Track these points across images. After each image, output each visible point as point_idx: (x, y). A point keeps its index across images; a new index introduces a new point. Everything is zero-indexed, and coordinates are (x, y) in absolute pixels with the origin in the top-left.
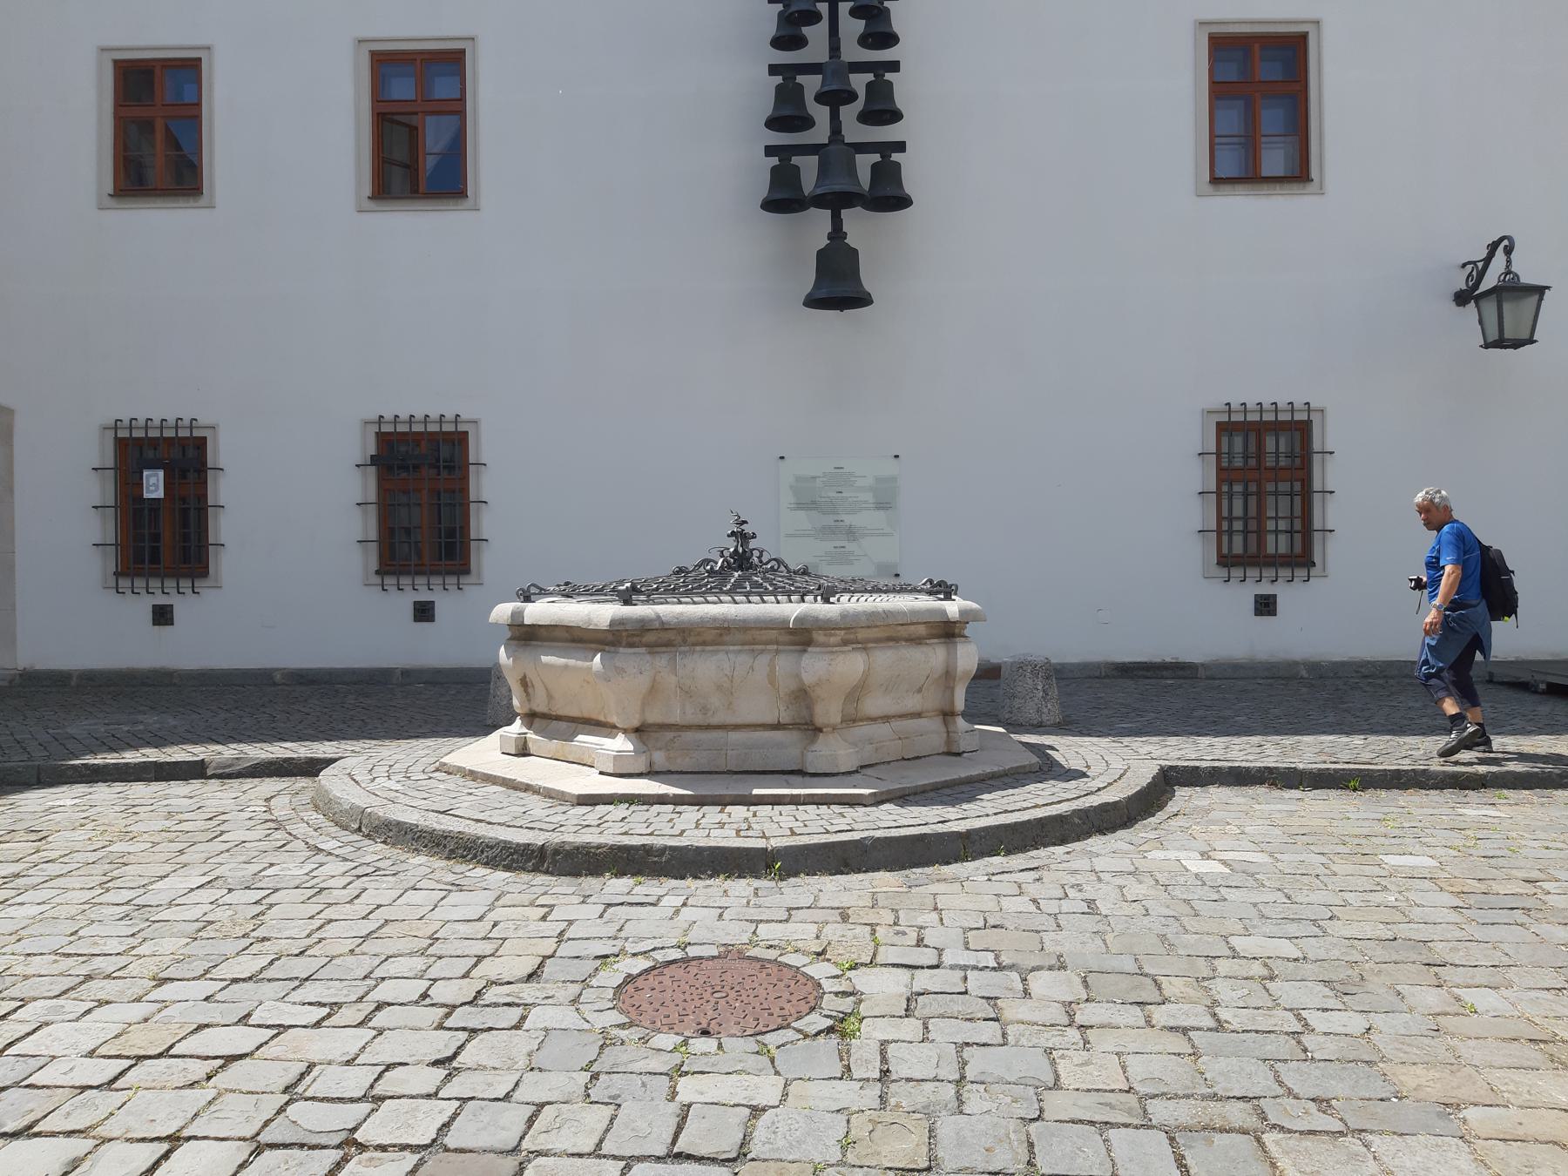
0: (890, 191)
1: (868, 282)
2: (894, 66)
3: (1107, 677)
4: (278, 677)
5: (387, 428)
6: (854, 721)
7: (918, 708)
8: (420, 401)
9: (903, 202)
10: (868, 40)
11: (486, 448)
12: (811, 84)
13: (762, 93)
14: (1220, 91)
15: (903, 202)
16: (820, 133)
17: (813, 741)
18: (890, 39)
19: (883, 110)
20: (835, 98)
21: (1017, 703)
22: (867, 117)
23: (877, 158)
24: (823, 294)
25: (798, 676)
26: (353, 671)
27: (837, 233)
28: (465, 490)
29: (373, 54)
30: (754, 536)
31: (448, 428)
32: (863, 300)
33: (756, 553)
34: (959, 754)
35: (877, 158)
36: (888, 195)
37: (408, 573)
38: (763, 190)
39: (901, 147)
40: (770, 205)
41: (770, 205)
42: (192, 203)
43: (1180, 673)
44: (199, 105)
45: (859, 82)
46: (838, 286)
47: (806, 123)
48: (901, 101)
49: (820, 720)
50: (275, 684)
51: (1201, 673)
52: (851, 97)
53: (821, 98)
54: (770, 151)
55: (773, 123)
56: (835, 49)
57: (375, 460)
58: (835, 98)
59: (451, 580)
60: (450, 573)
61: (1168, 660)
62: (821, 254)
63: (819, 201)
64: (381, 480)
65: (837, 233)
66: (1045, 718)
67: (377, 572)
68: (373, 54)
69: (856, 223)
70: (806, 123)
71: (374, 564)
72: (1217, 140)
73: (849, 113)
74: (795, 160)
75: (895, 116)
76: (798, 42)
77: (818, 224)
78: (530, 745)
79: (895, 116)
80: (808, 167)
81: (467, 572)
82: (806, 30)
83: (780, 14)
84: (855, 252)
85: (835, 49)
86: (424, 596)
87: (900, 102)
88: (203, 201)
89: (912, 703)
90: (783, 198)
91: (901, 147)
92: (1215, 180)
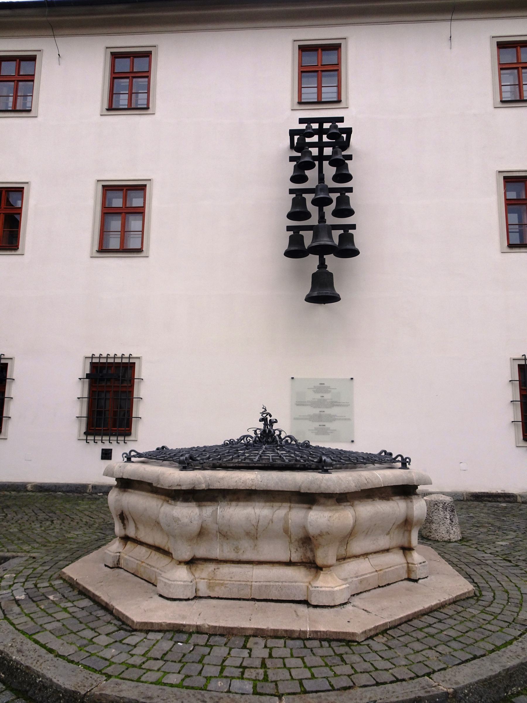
0: (349, 247)
1: (338, 289)
2: (350, 190)
3: (468, 500)
4: (29, 487)
5: (95, 361)
6: (344, 559)
7: (387, 547)
8: (112, 348)
9: (355, 253)
10: (337, 178)
11: (143, 371)
12: (309, 197)
13: (286, 203)
14: (510, 204)
15: (355, 253)
16: (314, 220)
17: (316, 576)
18: (348, 178)
19: (344, 210)
20: (321, 203)
21: (434, 526)
22: (337, 213)
23: (342, 232)
24: (315, 294)
25: (313, 579)
26: (68, 485)
27: (322, 265)
28: (131, 392)
29: (104, 186)
30: (276, 421)
31: (125, 361)
32: (335, 298)
33: (277, 433)
34: (416, 581)
35: (342, 232)
36: (347, 250)
37: (99, 435)
38: (285, 245)
39: (353, 227)
40: (289, 254)
41: (289, 254)
42: (13, 253)
43: (507, 499)
44: (21, 208)
45: (334, 196)
46: (323, 292)
47: (307, 215)
48: (353, 205)
49: (320, 561)
50: (27, 491)
51: (519, 499)
52: (330, 201)
53: (314, 202)
54: (291, 191)
55: (291, 216)
56: (321, 178)
57: (88, 376)
58: (321, 203)
59: (121, 438)
60: (121, 435)
61: (499, 491)
62: (314, 276)
63: (313, 250)
64: (91, 386)
65: (322, 265)
66: (452, 536)
67: (85, 433)
68: (104, 186)
69: (330, 259)
70: (307, 215)
71: (84, 429)
72: (510, 227)
73: (328, 210)
74: (301, 233)
75: (350, 212)
76: (304, 179)
77: (313, 261)
78: (122, 561)
79: (350, 212)
80: (308, 237)
81: (129, 434)
82: (307, 173)
83: (295, 166)
84: (331, 274)
85: (321, 178)
86: (107, 446)
87: (353, 205)
88: (18, 252)
89: (384, 542)
90: (295, 251)
91: (353, 227)
92: (511, 246)
